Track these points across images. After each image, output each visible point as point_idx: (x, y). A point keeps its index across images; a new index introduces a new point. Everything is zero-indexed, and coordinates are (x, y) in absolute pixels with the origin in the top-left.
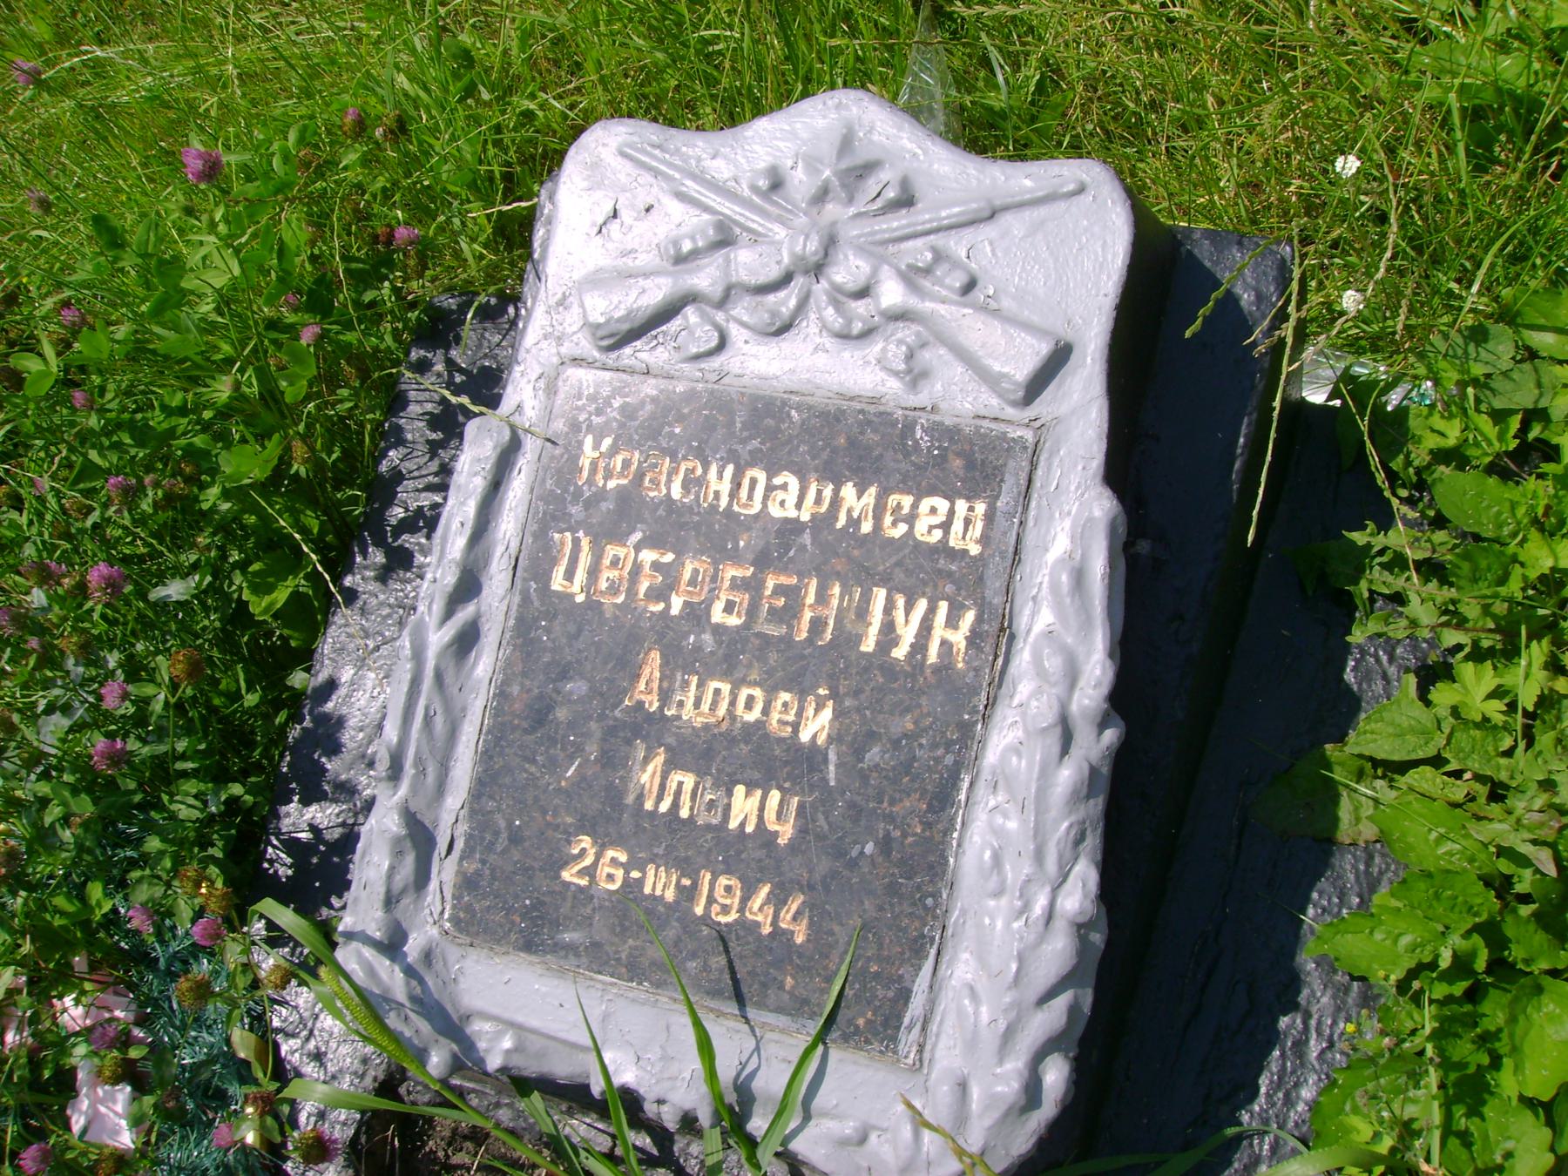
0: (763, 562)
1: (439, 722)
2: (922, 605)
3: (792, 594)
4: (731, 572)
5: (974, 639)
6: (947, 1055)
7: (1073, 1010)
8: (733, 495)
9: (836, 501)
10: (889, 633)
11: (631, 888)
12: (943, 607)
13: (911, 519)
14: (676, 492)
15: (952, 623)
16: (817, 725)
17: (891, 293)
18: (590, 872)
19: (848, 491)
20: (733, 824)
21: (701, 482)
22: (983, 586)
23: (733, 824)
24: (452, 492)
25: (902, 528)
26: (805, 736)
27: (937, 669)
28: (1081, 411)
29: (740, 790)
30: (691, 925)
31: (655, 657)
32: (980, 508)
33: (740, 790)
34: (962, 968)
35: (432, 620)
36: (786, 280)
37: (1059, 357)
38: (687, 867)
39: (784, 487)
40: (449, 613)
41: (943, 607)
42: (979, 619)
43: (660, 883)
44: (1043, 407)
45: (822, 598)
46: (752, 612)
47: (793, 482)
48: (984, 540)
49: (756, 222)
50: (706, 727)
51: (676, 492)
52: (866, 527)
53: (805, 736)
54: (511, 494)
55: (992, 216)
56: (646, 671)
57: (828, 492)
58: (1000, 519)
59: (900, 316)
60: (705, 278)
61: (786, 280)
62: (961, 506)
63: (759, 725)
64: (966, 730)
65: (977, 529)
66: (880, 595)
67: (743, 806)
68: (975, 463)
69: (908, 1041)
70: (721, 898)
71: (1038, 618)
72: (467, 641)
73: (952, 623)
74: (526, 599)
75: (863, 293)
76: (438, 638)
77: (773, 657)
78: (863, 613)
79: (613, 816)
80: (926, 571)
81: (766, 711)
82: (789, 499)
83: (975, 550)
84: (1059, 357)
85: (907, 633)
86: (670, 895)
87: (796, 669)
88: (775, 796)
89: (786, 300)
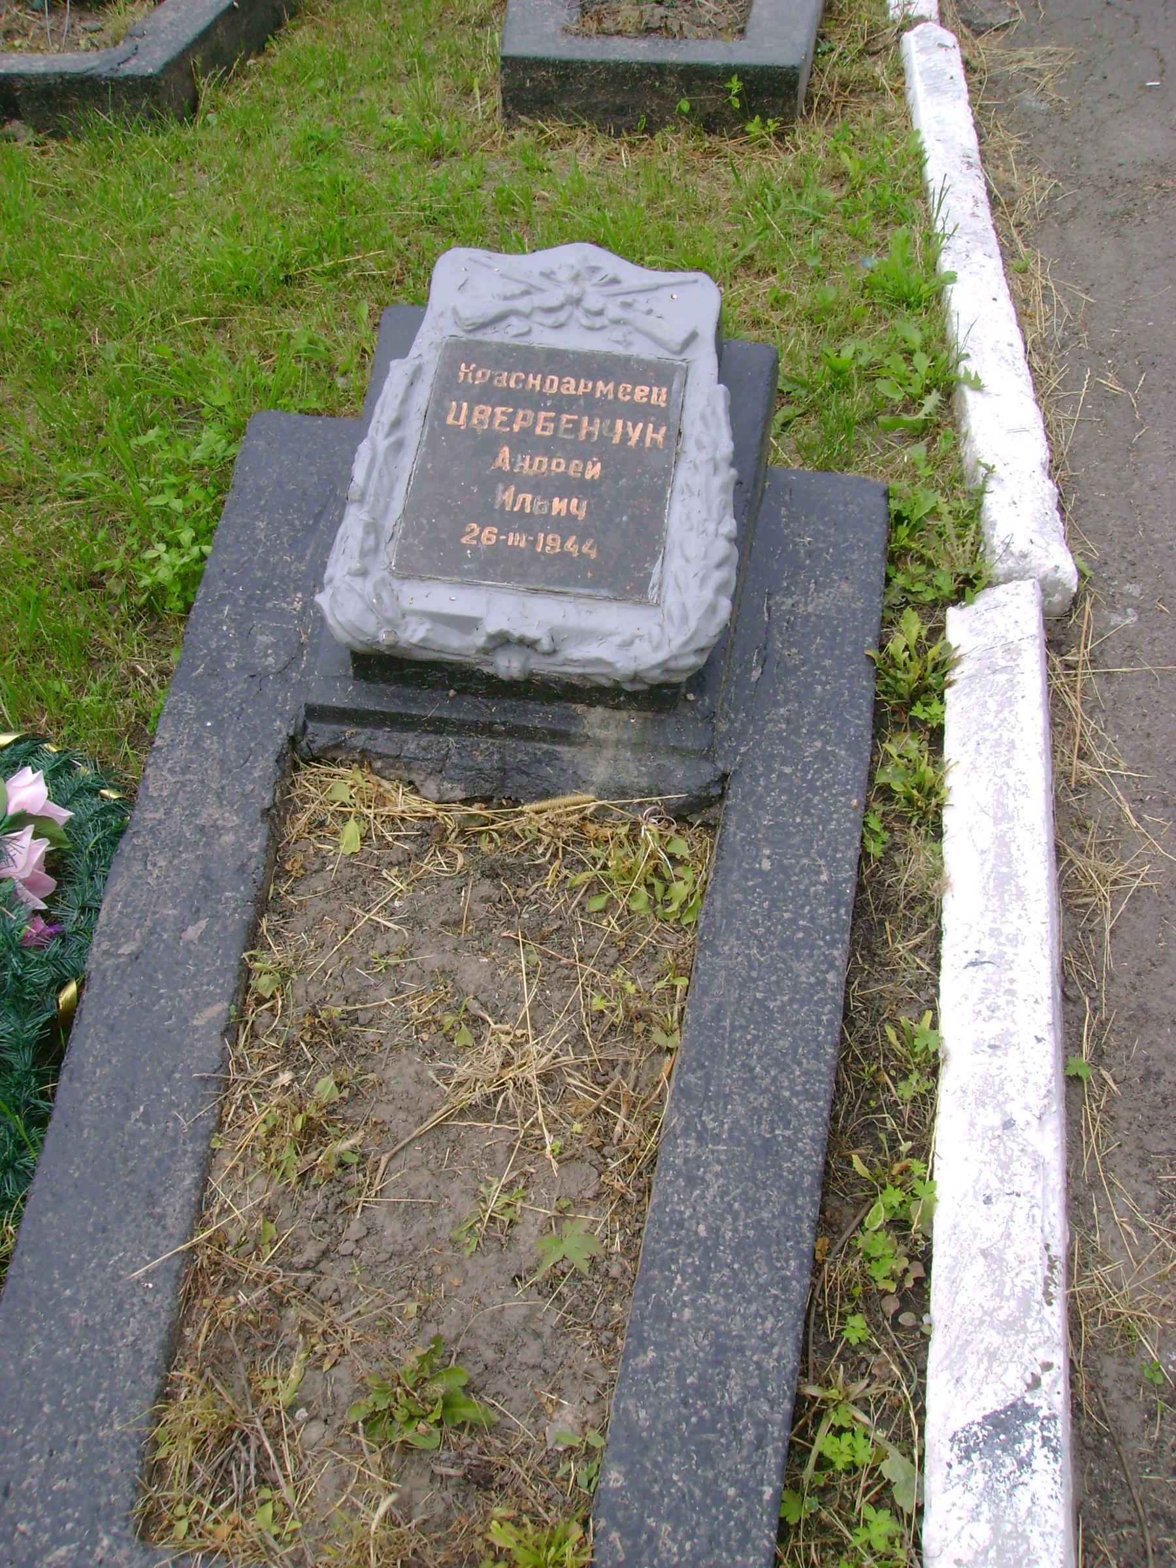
0: (559, 411)
2: (640, 425)
3: (577, 424)
4: (542, 415)
5: (667, 437)
6: (671, 600)
8: (542, 386)
9: (594, 388)
10: (625, 437)
12: (651, 426)
13: (632, 393)
14: (512, 384)
15: (656, 431)
17: (614, 311)
18: (478, 538)
19: (600, 384)
20: (554, 513)
21: (525, 381)
22: (670, 419)
23: (554, 513)
25: (628, 398)
26: (588, 476)
27: (650, 449)
28: (704, 360)
29: (556, 500)
30: (536, 557)
31: (506, 449)
32: (664, 390)
33: (556, 500)
34: (675, 563)
36: (561, 307)
38: (530, 531)
40: (388, 435)
41: (651, 426)
42: (668, 429)
44: (687, 355)
45: (591, 423)
46: (556, 430)
47: (573, 381)
48: (667, 401)
50: (536, 476)
51: (512, 384)
52: (611, 397)
53: (588, 476)
56: (501, 457)
57: (590, 385)
58: (674, 395)
59: (617, 322)
60: (523, 304)
61: (561, 307)
62: (655, 390)
63: (565, 474)
64: (667, 472)
65: (663, 397)
66: (619, 423)
67: (558, 505)
68: (662, 374)
69: (652, 594)
70: (548, 543)
71: (692, 425)
72: (399, 446)
74: (432, 429)
76: (383, 444)
77: (569, 447)
78: (612, 428)
79: (489, 515)
80: (638, 412)
81: (567, 467)
82: (570, 386)
83: (663, 405)
85: (635, 435)
86: (522, 544)
87: (583, 451)
88: (575, 501)
89: (562, 316)
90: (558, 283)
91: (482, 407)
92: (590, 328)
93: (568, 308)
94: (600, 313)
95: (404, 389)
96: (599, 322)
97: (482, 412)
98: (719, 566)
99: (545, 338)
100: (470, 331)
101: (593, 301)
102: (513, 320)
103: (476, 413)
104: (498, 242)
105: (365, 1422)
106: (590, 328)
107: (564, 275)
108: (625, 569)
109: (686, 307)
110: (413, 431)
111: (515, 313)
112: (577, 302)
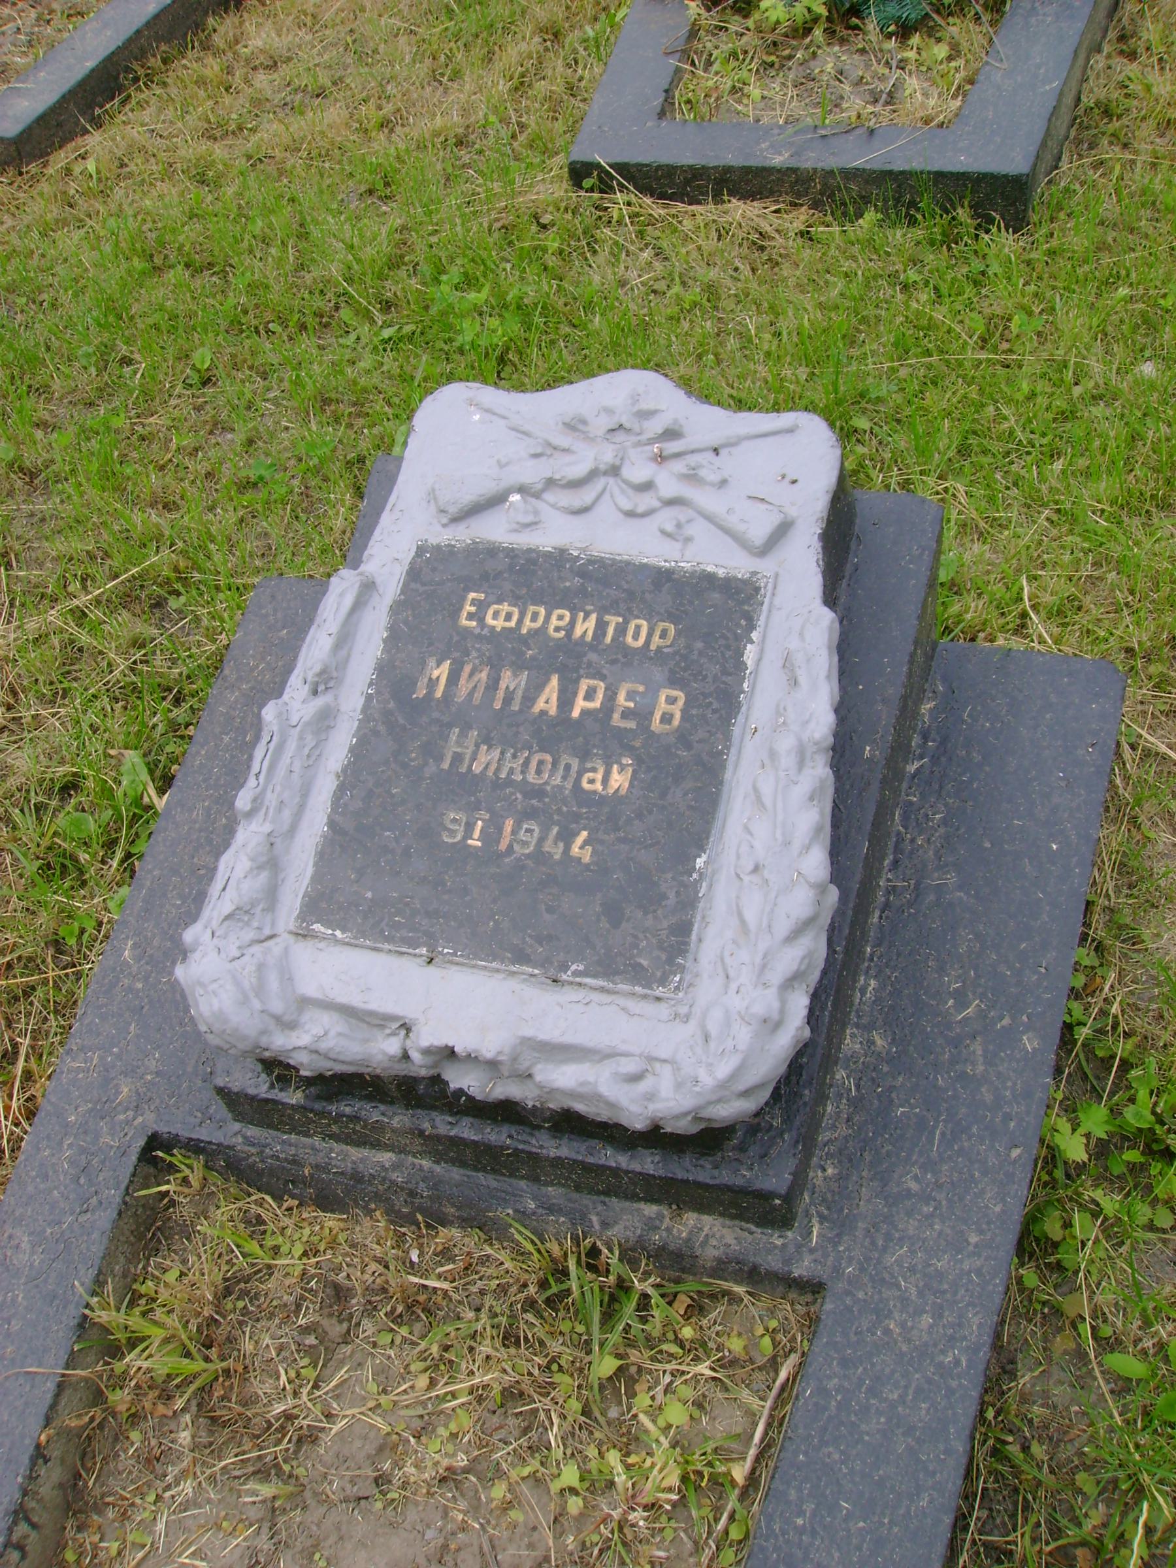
7: (809, 955)
17: (668, 483)
28: (798, 574)
37: (783, 529)
84: (783, 529)
89: (586, 496)
90: (589, 439)
91: (560, 611)
92: (631, 514)
93: (601, 483)
94: (647, 487)
95: (348, 630)
96: (646, 501)
97: (561, 618)
98: (746, 1094)
99: (556, 532)
100: (455, 520)
101: (638, 470)
103: (554, 618)
104: (504, 367)
105: (142, 812)
106: (631, 514)
107: (600, 425)
108: (627, 914)
109: (789, 464)
110: (352, 699)
112: (614, 471)
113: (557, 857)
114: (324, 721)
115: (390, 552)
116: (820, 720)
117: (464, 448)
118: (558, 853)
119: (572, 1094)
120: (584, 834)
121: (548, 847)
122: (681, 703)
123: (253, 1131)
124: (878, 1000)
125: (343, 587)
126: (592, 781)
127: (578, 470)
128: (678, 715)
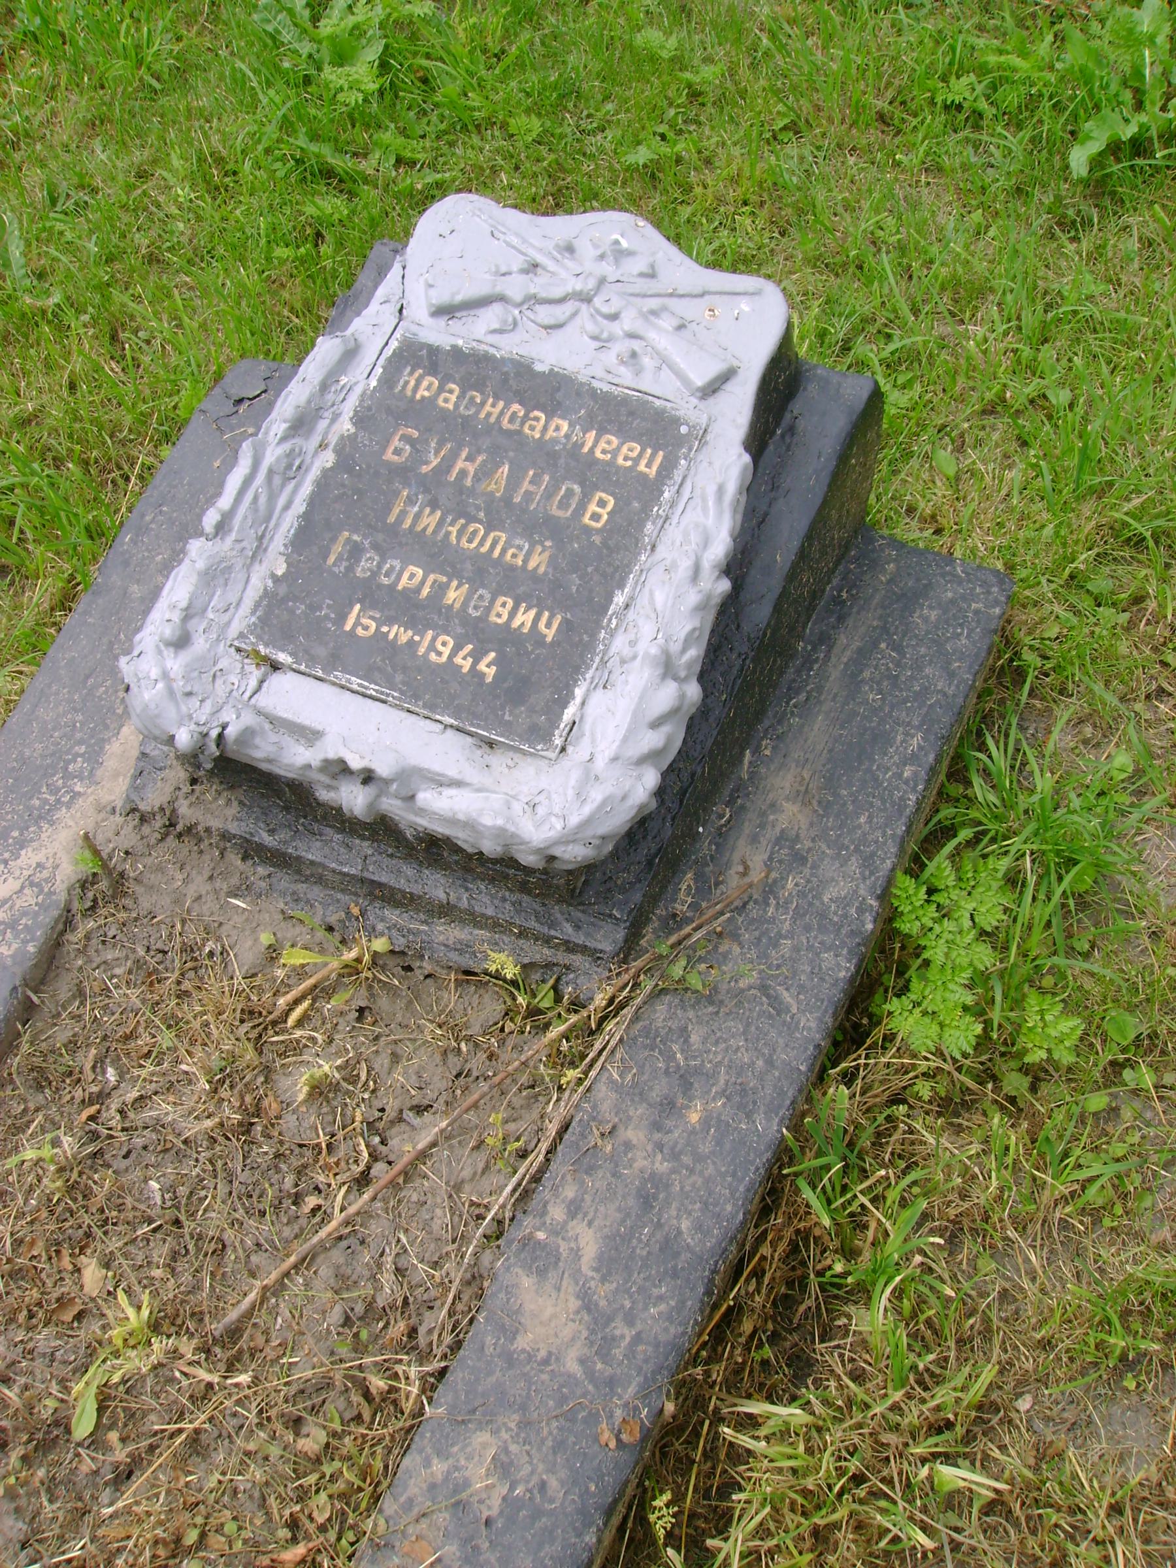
1: (263, 500)
7: (669, 740)
11: (379, 636)
16: (538, 561)
24: (135, 753)
28: (736, 410)
35: (272, 439)
37: (727, 376)
39: (626, 459)
43: (399, 633)
49: (551, 265)
54: (440, 830)
55: (702, 295)
60: (516, 287)
73: (489, 414)
75: (614, 317)
76: (272, 455)
84: (727, 376)
98: (655, 725)
102: (497, 308)
108: (520, 701)
109: (750, 320)
111: (502, 299)
112: (588, 300)
113: (465, 670)
114: (291, 469)
115: (373, 327)
116: (720, 546)
117: (463, 258)
118: (466, 665)
119: (453, 821)
120: (493, 655)
121: (458, 660)
122: (610, 507)
123: (353, 401)
124: (662, 1492)
125: (326, 349)
126: (631, 450)
127: (558, 293)
128: (605, 517)
